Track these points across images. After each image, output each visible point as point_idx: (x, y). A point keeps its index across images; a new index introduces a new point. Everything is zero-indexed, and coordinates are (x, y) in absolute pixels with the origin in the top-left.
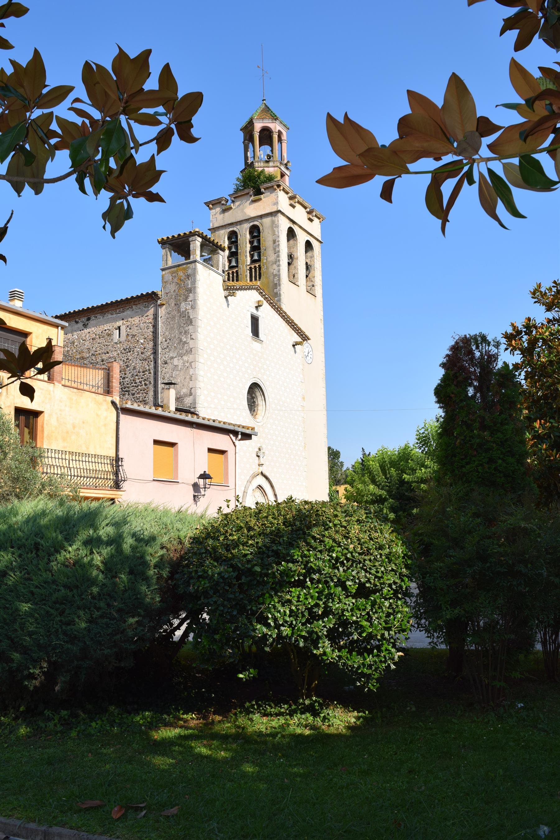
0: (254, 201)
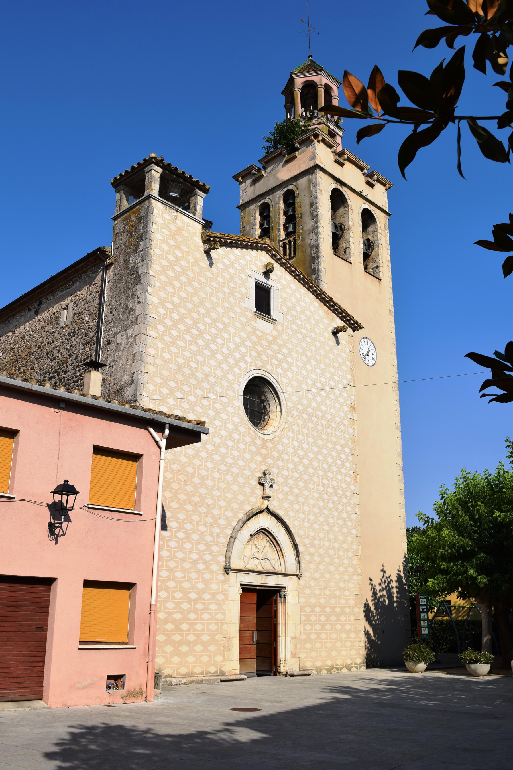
0: (288, 161)
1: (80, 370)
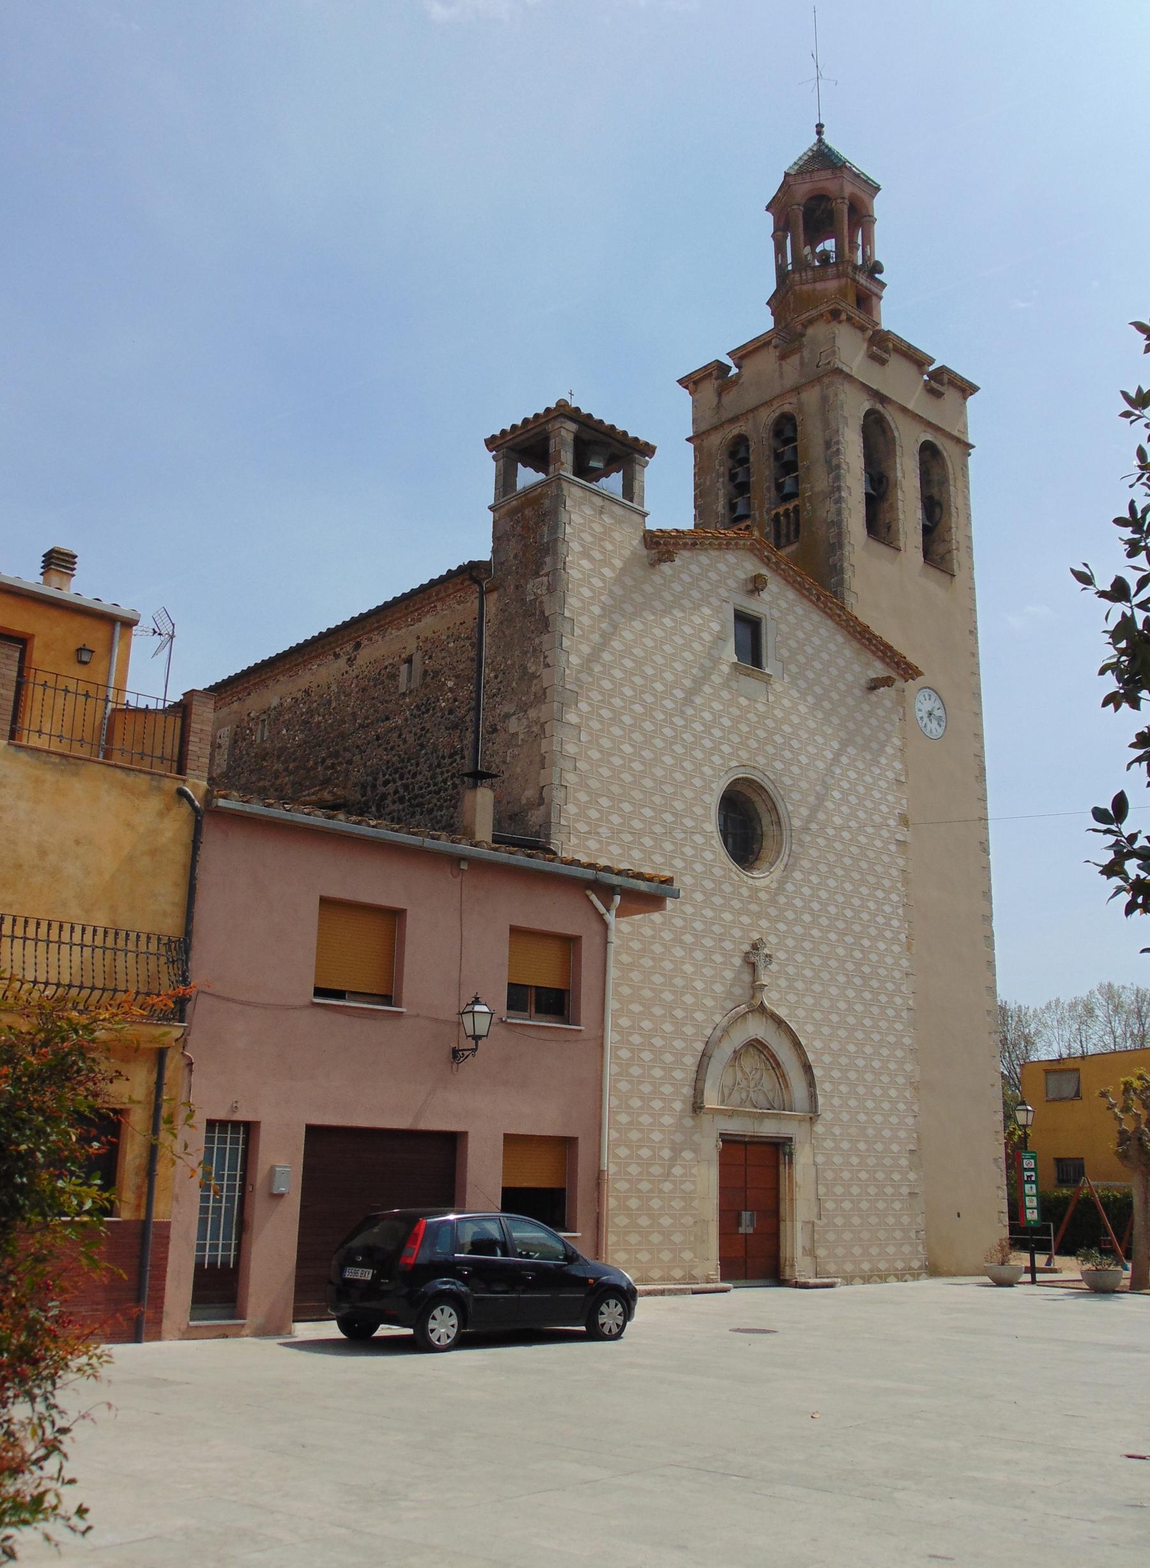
1: (442, 773)
